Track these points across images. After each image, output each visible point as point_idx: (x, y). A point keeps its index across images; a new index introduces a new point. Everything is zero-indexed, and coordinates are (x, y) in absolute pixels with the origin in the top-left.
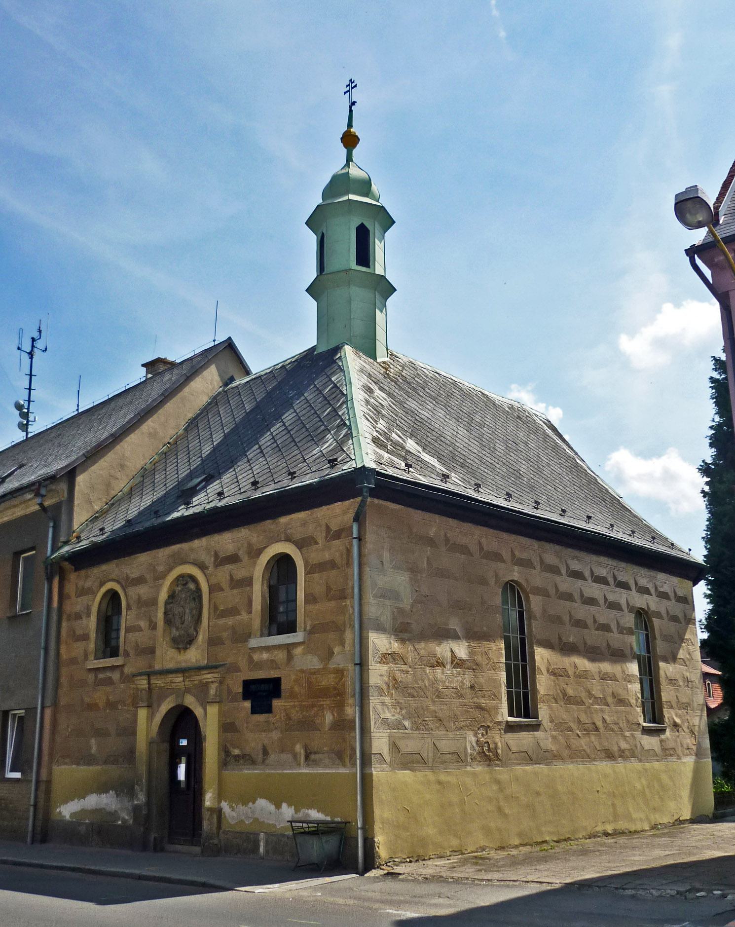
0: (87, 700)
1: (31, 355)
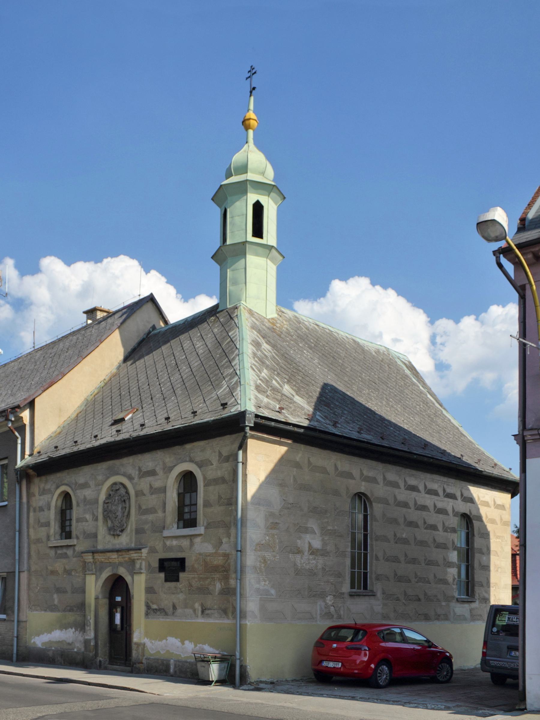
0: (50, 568)
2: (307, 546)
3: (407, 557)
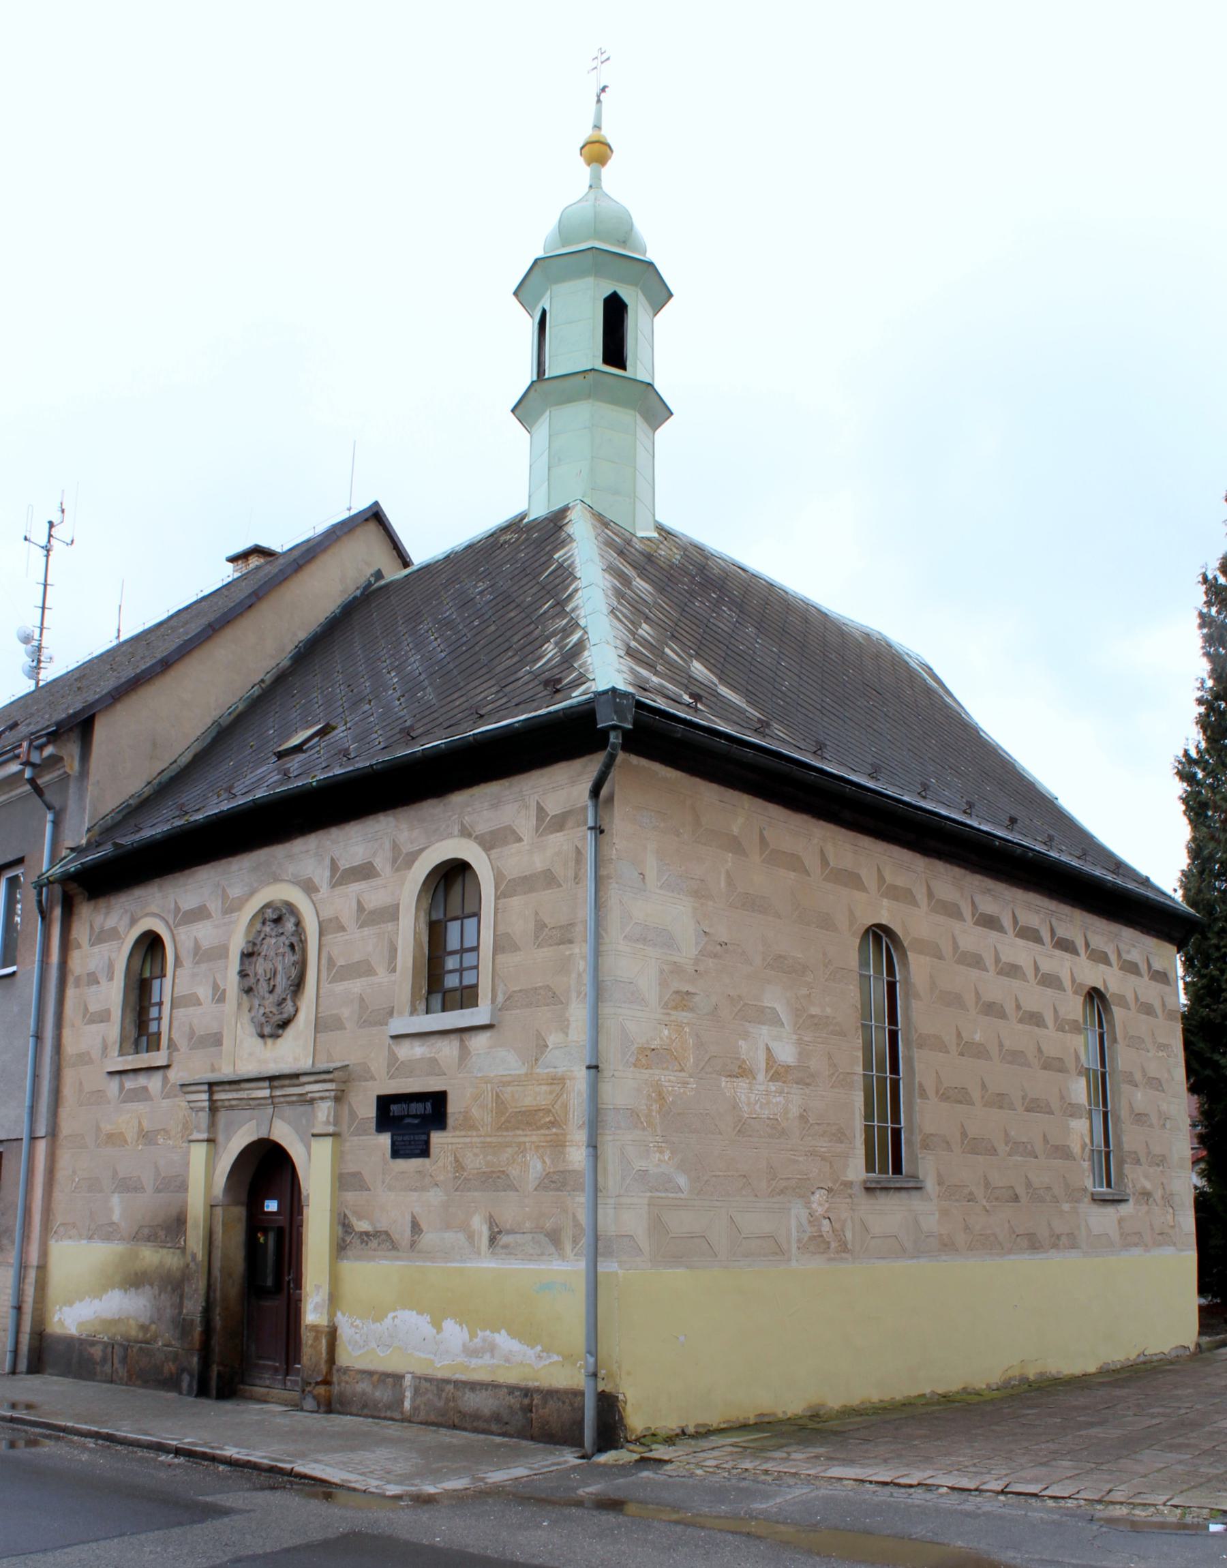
0: (107, 1127)
1: (48, 550)
2: (762, 1056)
3: (987, 1091)
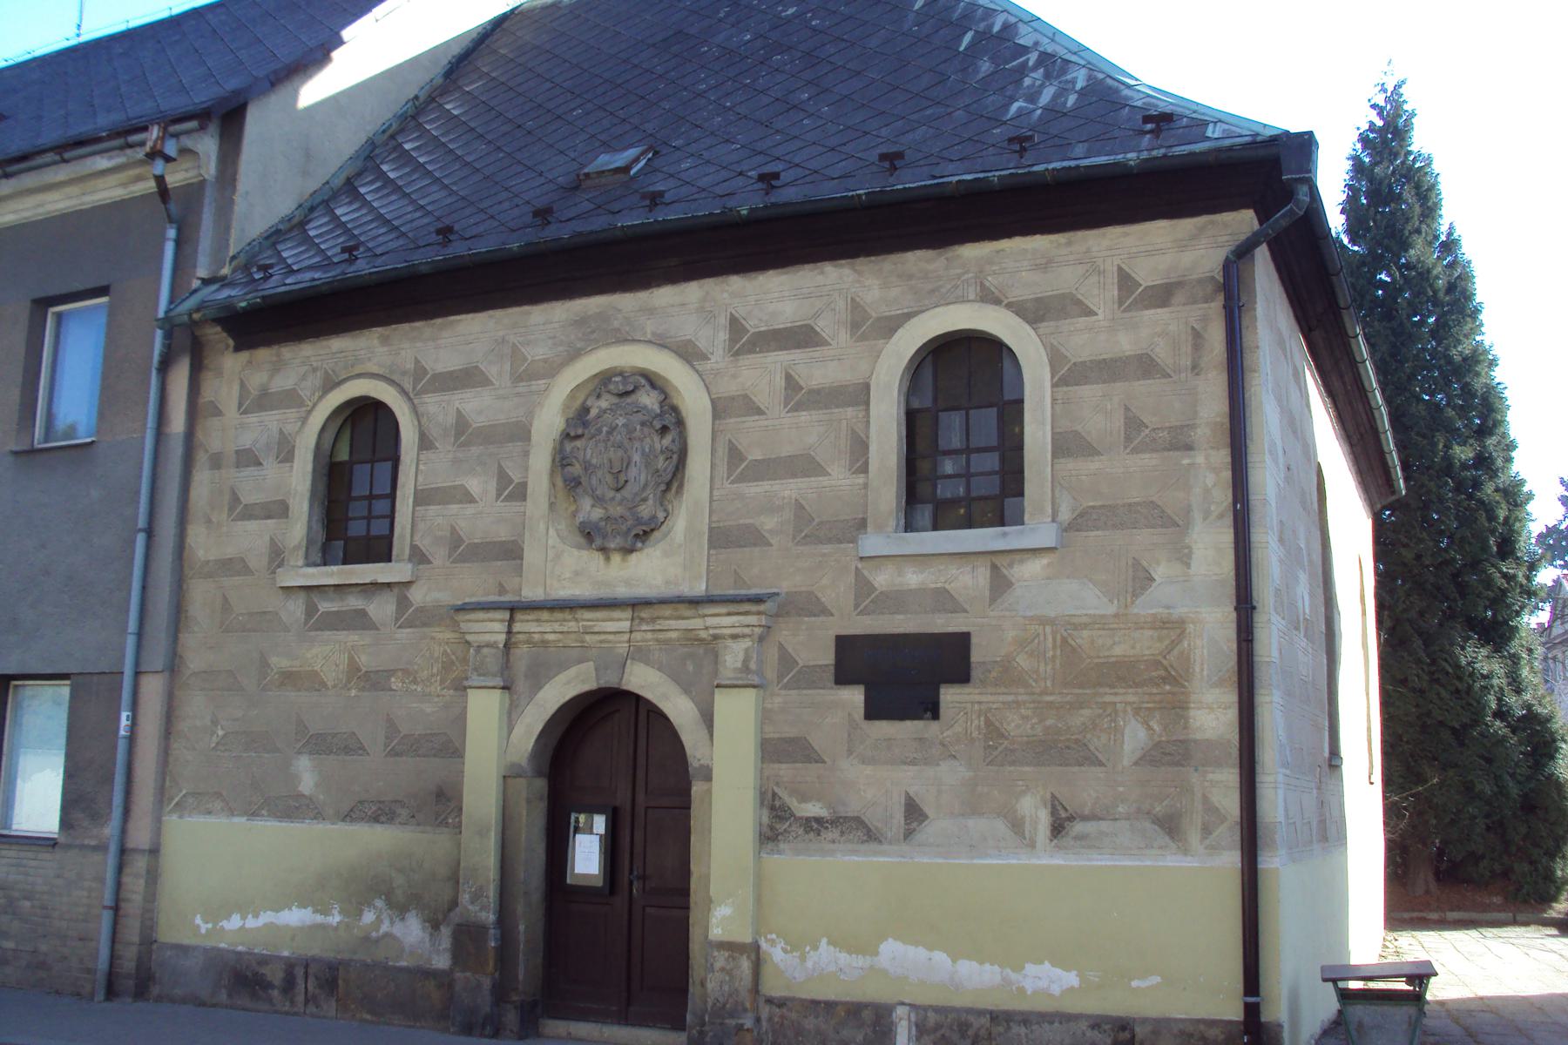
0: (279, 662)
